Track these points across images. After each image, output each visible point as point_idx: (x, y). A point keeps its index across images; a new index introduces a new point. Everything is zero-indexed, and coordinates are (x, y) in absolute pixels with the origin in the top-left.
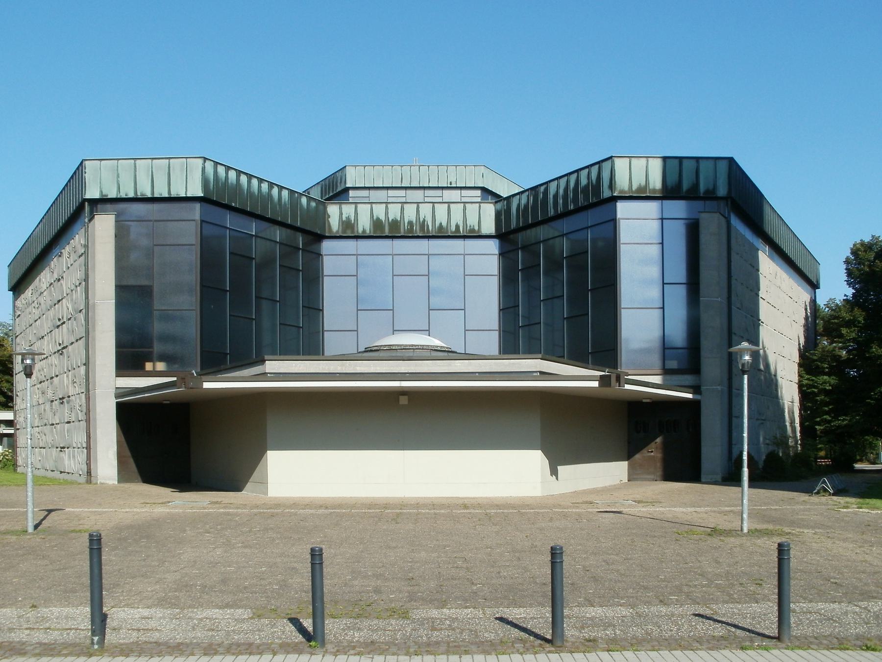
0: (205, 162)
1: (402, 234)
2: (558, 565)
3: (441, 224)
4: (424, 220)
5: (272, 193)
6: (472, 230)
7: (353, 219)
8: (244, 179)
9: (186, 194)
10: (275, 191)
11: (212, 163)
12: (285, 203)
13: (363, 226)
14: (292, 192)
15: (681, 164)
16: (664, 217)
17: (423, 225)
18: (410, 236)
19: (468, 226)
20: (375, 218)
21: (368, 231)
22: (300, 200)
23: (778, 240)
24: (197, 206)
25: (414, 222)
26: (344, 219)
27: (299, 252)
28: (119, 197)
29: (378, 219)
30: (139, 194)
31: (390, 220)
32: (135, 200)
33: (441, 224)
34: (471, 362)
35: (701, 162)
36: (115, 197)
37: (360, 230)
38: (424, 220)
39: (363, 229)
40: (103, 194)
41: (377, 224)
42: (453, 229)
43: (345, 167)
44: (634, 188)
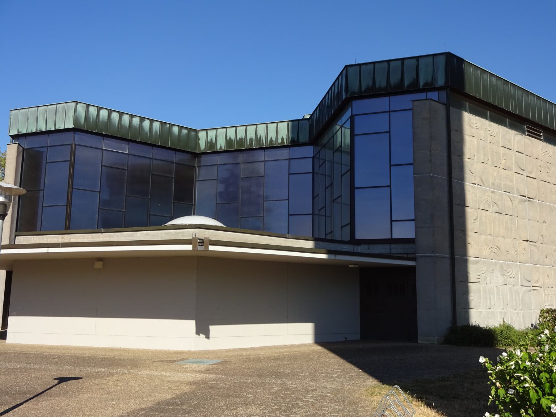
0: (77, 104)
1: (246, 147)
3: (271, 138)
4: (260, 137)
5: (143, 124)
7: (214, 142)
8: (115, 116)
9: (55, 128)
10: (146, 124)
11: (96, 108)
12: (156, 132)
13: (221, 144)
14: (162, 124)
17: (258, 140)
20: (228, 138)
21: (223, 148)
22: (172, 129)
25: (254, 138)
27: (174, 164)
28: (27, 132)
29: (230, 138)
30: (38, 130)
33: (271, 138)
34: (205, 232)
36: (16, 134)
37: (218, 147)
38: (260, 137)
39: (221, 146)
40: (19, 131)
41: (229, 142)
42: (280, 141)
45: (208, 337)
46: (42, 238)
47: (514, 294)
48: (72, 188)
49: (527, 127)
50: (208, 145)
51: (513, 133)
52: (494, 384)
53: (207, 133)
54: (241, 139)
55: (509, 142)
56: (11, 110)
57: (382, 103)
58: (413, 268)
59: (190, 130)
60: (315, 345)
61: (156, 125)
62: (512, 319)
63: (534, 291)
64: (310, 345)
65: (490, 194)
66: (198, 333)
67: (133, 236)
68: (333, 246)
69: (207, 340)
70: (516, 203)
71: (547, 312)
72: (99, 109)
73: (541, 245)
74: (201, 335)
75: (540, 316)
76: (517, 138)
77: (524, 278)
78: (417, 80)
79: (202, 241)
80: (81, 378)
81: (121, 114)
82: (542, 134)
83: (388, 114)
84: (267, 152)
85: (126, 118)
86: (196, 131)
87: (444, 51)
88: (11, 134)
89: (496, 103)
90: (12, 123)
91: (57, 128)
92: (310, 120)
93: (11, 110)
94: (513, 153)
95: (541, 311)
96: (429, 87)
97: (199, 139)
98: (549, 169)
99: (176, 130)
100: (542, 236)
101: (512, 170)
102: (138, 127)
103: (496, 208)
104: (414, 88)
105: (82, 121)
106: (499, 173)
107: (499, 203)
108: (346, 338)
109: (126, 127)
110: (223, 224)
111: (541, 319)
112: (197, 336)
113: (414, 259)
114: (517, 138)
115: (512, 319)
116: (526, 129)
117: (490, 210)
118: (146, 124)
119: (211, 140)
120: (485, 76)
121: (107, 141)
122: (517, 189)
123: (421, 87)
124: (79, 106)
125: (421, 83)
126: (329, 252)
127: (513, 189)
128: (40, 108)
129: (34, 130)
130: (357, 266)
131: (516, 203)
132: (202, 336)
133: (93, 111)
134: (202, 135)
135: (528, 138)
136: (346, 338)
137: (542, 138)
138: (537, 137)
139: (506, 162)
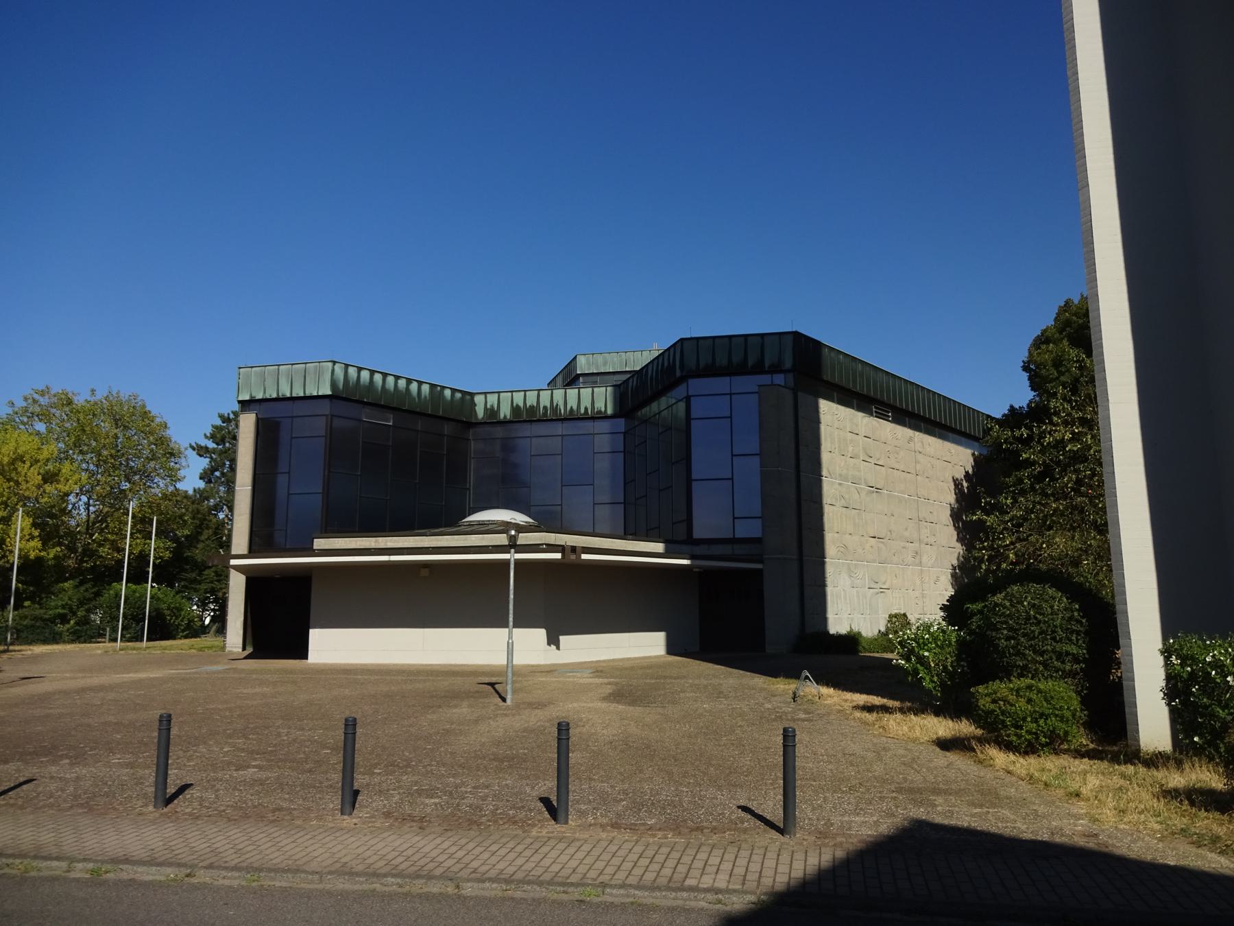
0: (334, 365)
1: (538, 417)
2: (790, 749)
3: (572, 407)
4: (557, 404)
6: (600, 412)
7: (496, 409)
8: (378, 378)
9: (305, 393)
10: (414, 386)
11: (356, 368)
12: (426, 397)
14: (433, 386)
15: (746, 341)
16: (732, 392)
17: (555, 409)
18: (544, 420)
19: (596, 408)
21: (508, 417)
22: (443, 393)
23: (919, 407)
24: (327, 401)
25: (549, 406)
26: (488, 406)
29: (517, 405)
30: (280, 394)
31: (528, 406)
32: (277, 400)
33: (572, 407)
34: (551, 536)
35: (701, 342)
37: (502, 416)
38: (557, 404)
41: (516, 410)
42: (582, 411)
43: (575, 357)
44: (702, 365)
45: (558, 648)
46: (350, 541)
47: (861, 598)
48: (329, 472)
49: (875, 408)
50: (488, 413)
51: (860, 414)
52: (897, 647)
53: (486, 398)
54: (532, 407)
55: (857, 426)
56: (240, 368)
57: (721, 384)
58: (760, 571)
59: (464, 393)
60: (667, 656)
61: (426, 389)
62: (859, 626)
63: (882, 594)
64: (661, 656)
65: (837, 486)
66: (549, 644)
67: (466, 540)
68: (698, 550)
69: (557, 651)
70: (863, 495)
71: (896, 617)
72: (360, 369)
73: (889, 541)
74: (552, 646)
75: (889, 621)
76: (864, 421)
77: (872, 579)
78: (761, 361)
79: (574, 549)
80: (555, 670)
81: (385, 375)
82: (890, 414)
83: (728, 397)
84: (566, 424)
85: (391, 380)
86: (472, 395)
87: (790, 330)
88: (240, 399)
89: (844, 384)
90: (242, 385)
91: (308, 394)
92: (622, 387)
93: (240, 368)
94: (860, 439)
95: (890, 615)
96: (776, 369)
97: (475, 405)
98: (898, 454)
99: (448, 393)
100: (890, 531)
101: (859, 458)
102: (404, 390)
103: (843, 502)
104: (758, 369)
105: (341, 386)
106: (846, 462)
107: (847, 496)
108: (686, 650)
109: (390, 391)
110: (527, 515)
111: (889, 625)
112: (548, 647)
113: (761, 561)
114: (864, 421)
115: (859, 626)
116: (874, 409)
117: (837, 505)
118: (414, 386)
119: (492, 406)
120: (833, 354)
121: (367, 410)
122: (865, 479)
123: (766, 369)
124: (337, 367)
125: (767, 364)
126: (691, 558)
127: (861, 479)
128: (281, 367)
129: (274, 396)
130: (701, 570)
131: (863, 495)
132: (553, 647)
133: (352, 372)
134: (479, 400)
135: (876, 420)
136: (686, 650)
137: (890, 419)
138: (885, 418)
139: (853, 450)
